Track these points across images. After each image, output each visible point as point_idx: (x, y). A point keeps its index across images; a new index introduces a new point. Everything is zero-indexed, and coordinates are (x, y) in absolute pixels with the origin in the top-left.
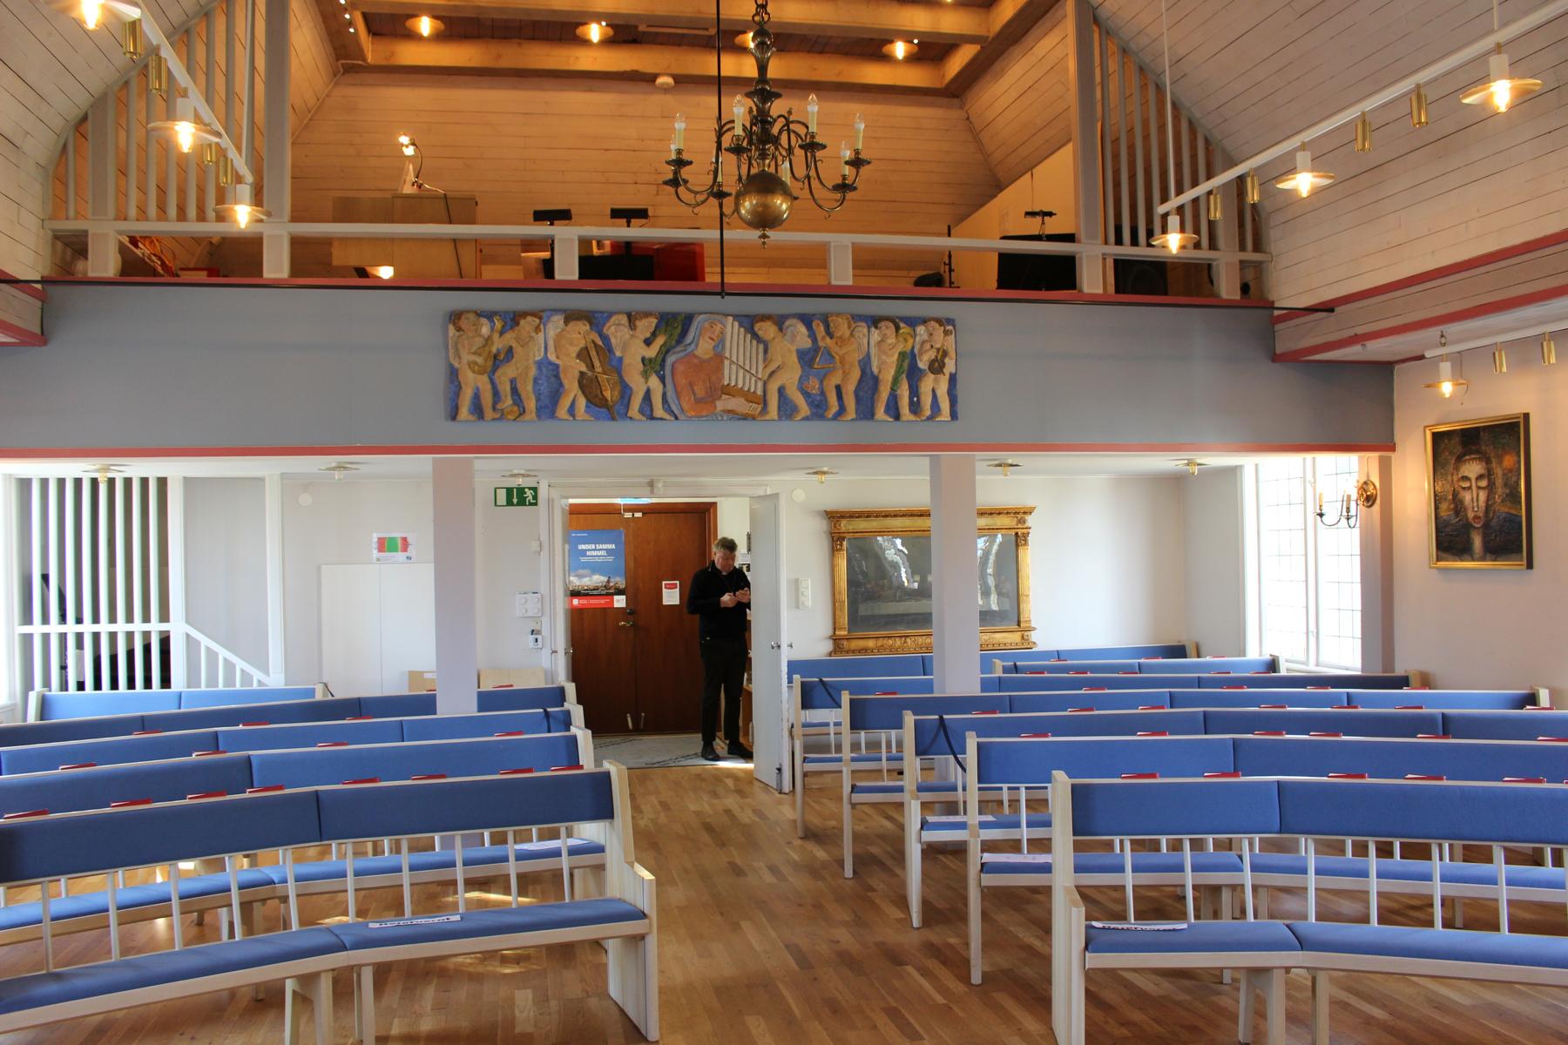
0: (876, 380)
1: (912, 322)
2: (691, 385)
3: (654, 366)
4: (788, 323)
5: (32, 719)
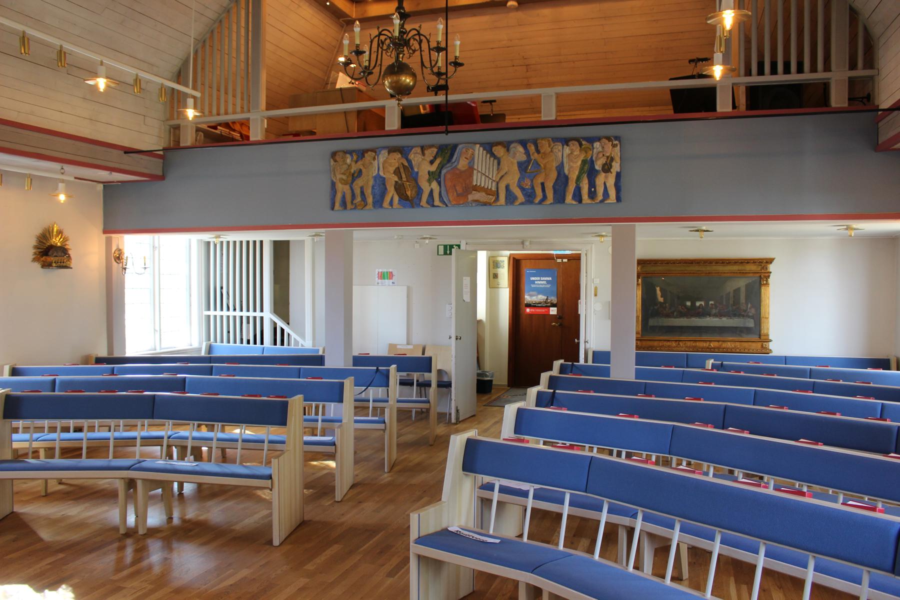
0: (567, 178)
1: (591, 140)
2: (455, 186)
3: (435, 176)
4: (512, 146)
5: (203, 354)
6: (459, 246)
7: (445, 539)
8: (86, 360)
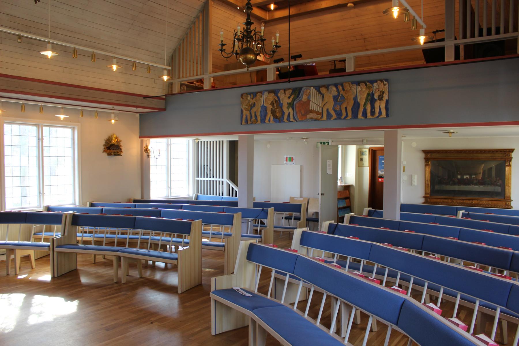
1: (372, 82)
3: (291, 105)
4: (330, 87)
5: (193, 200)
6: (328, 143)
7: (230, 293)
8: (129, 201)
